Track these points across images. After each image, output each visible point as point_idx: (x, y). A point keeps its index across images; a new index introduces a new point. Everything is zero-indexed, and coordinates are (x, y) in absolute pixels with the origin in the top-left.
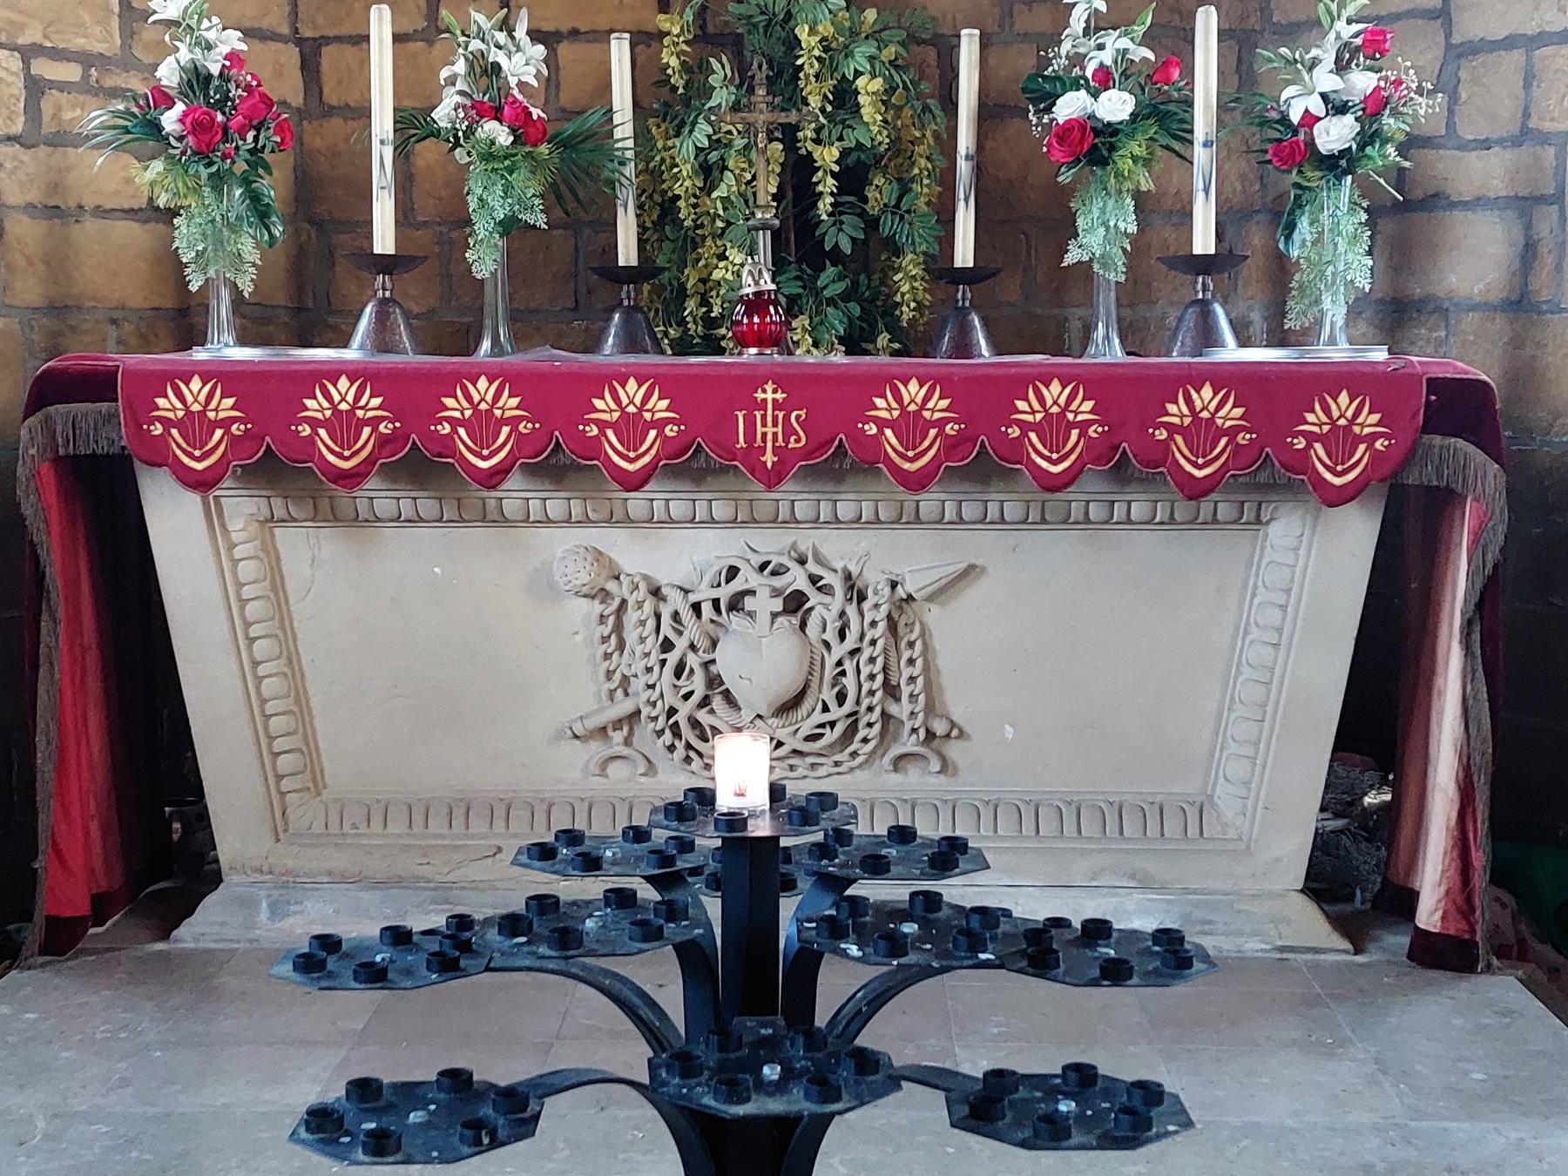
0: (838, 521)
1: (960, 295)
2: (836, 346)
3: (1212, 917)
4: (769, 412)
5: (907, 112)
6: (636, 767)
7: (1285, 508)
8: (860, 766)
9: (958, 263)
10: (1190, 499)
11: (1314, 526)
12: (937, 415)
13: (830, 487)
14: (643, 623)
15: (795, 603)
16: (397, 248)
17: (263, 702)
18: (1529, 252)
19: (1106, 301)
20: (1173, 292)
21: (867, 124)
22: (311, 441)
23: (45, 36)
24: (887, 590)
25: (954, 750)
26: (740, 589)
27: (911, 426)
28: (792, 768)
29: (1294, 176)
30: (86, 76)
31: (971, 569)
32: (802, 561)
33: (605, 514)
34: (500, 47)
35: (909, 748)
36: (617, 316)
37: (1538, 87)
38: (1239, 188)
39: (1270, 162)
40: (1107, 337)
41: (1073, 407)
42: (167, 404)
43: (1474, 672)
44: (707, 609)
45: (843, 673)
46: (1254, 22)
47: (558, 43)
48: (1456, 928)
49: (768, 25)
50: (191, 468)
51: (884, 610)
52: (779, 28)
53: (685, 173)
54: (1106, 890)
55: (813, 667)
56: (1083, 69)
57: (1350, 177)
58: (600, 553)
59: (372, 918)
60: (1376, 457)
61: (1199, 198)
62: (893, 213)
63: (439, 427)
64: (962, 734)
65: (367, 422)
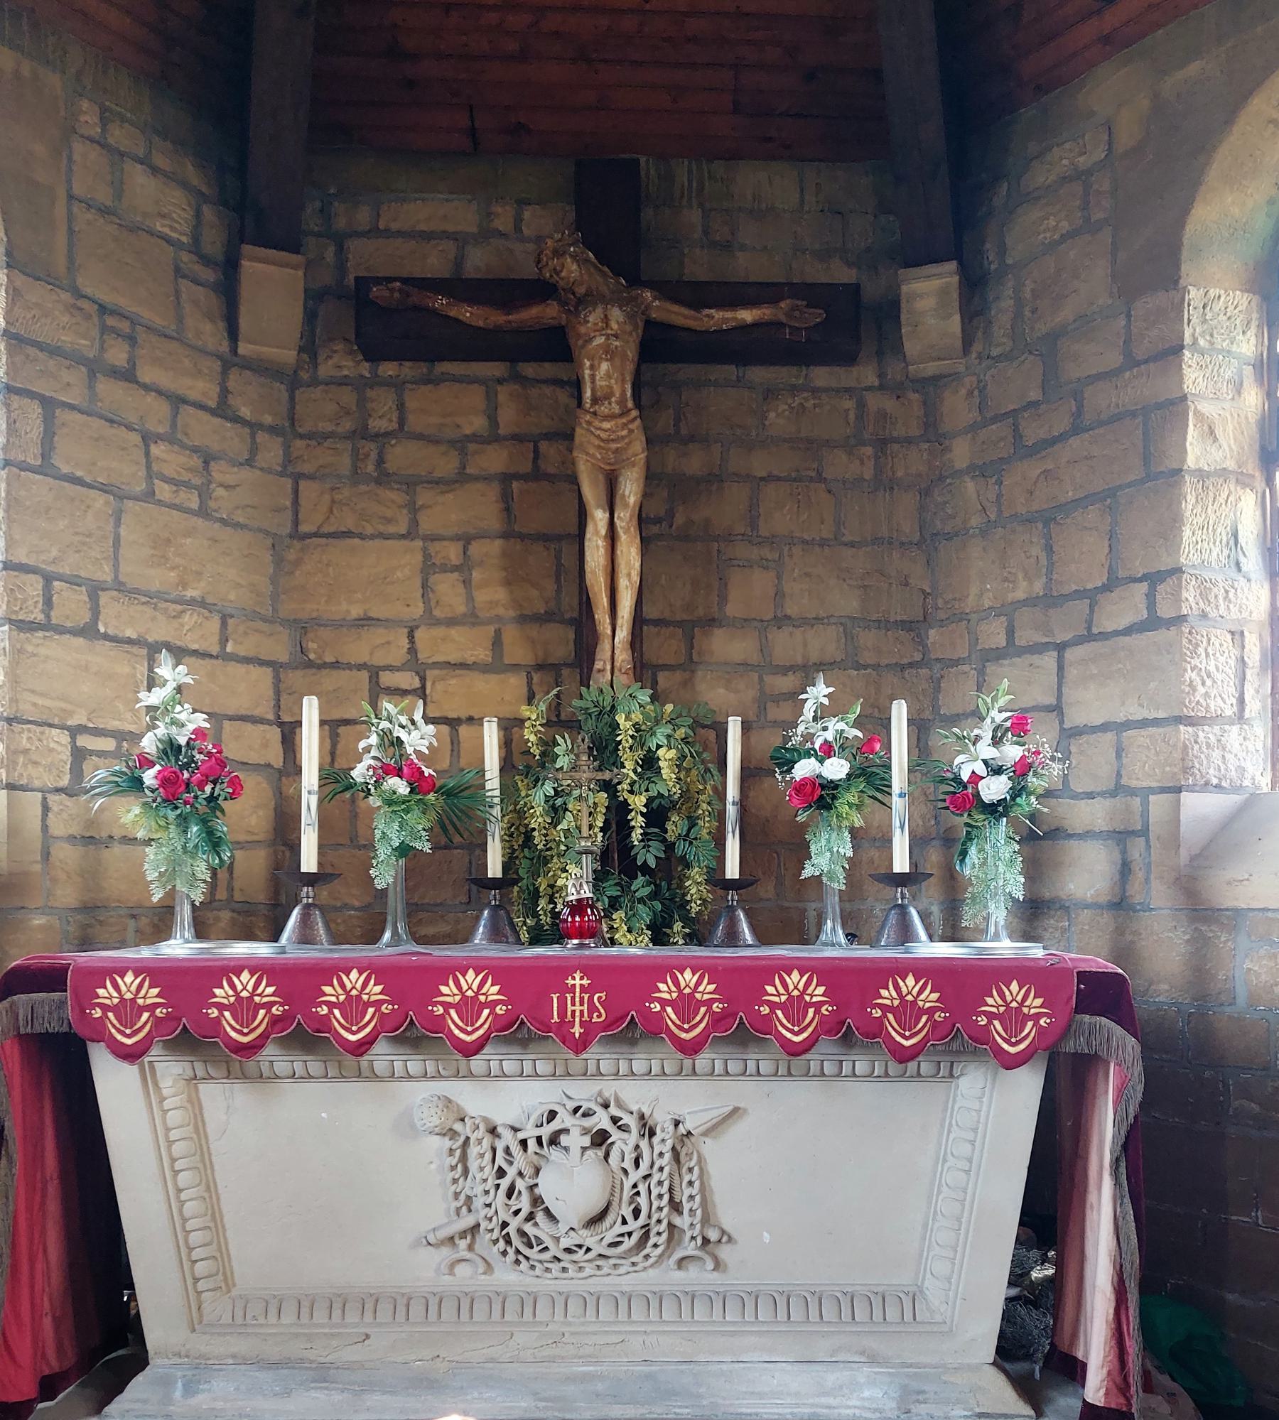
0: (633, 1074)
1: (730, 898)
2: (645, 931)
3: (925, 1388)
4: (577, 994)
5: (694, 772)
6: (477, 1267)
7: (972, 1066)
8: (652, 1266)
9: (728, 876)
10: (901, 1063)
11: (994, 1080)
12: (706, 997)
13: (625, 1048)
14: (482, 1155)
15: (600, 1139)
16: (320, 864)
17: (185, 1220)
18: (1125, 870)
19: (833, 904)
20: (878, 900)
21: (666, 780)
22: (217, 1021)
23: (89, 720)
24: (672, 1128)
25: (724, 1252)
26: (557, 1128)
27: (686, 1005)
28: (598, 1267)
29: (965, 818)
30: (119, 747)
31: (736, 1110)
32: (606, 1106)
33: (453, 1071)
34: (403, 727)
35: (690, 1252)
36: (486, 912)
37: (1126, 757)
38: (921, 823)
39: (947, 808)
40: (834, 929)
41: (809, 991)
42: (106, 994)
43: (1122, 1197)
44: (532, 1144)
45: (638, 1193)
46: (927, 714)
47: (459, 725)
48: (1117, 1402)
49: (600, 714)
50: (122, 1043)
51: (669, 1144)
52: (606, 716)
53: (538, 813)
54: (842, 1365)
55: (614, 1190)
56: (813, 743)
57: (1005, 819)
58: (450, 1101)
59: (265, 1395)
60: (1041, 1032)
61: (897, 832)
62: (684, 840)
63: (319, 1009)
64: (730, 1240)
65: (263, 1006)
